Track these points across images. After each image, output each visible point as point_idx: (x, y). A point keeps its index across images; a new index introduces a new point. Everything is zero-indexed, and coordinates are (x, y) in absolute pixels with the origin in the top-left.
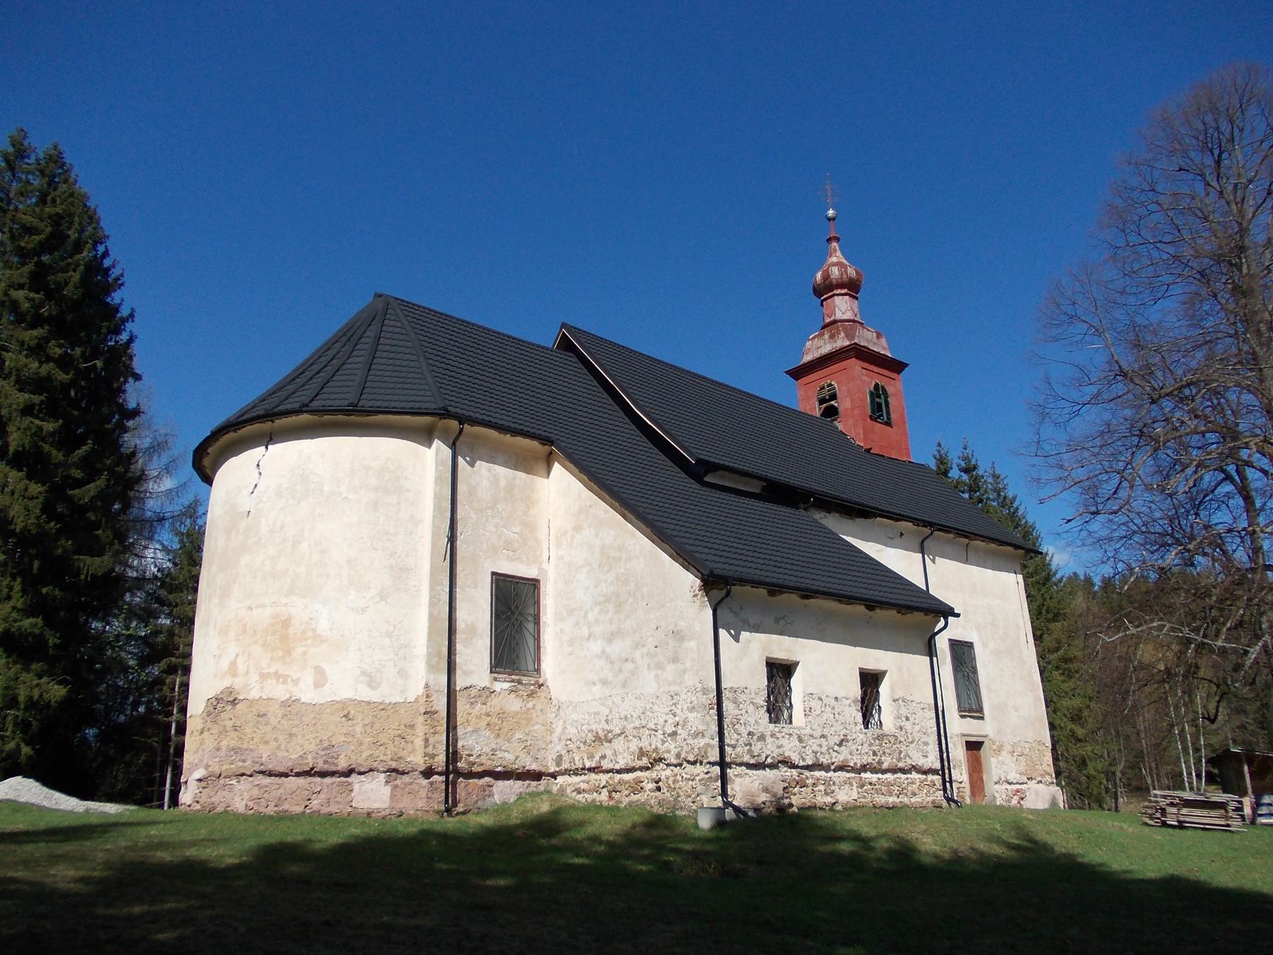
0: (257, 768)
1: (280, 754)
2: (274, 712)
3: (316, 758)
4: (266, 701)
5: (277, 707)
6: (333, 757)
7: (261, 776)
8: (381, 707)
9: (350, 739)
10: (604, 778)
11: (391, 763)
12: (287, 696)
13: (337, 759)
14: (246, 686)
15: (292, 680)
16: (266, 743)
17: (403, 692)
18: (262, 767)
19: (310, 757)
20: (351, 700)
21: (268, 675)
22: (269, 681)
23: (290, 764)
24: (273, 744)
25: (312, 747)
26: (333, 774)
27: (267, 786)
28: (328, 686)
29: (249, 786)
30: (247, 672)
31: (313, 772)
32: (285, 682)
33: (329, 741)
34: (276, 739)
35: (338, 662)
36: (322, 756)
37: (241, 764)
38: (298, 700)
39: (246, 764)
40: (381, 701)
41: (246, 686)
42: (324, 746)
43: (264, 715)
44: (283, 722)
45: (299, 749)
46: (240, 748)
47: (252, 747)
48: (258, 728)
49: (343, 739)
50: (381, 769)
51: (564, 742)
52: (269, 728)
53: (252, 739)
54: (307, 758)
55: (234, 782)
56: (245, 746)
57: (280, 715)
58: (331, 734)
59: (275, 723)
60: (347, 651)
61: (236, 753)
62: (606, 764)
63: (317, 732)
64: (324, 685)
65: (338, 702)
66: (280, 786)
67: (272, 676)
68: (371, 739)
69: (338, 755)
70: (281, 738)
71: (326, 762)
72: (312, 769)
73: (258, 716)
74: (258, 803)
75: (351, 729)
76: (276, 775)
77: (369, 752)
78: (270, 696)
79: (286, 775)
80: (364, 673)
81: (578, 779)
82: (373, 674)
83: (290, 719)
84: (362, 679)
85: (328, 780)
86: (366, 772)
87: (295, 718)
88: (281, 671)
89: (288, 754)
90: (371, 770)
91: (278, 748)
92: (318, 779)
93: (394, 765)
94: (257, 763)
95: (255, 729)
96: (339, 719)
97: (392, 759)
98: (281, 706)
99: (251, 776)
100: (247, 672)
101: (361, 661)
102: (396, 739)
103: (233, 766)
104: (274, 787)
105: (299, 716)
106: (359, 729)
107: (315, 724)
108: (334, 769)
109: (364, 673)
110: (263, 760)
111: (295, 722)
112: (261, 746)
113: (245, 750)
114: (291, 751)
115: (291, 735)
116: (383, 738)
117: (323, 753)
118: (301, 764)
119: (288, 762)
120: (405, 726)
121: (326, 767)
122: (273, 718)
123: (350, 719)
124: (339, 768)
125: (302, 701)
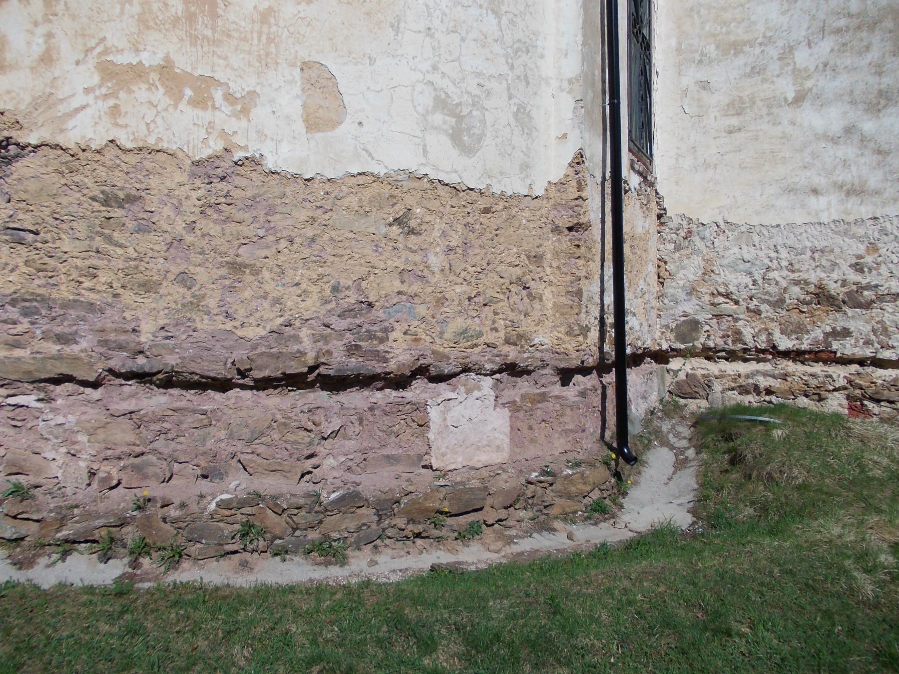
0: (119, 361)
1: (204, 324)
2: (170, 193)
3: (325, 338)
4: (132, 159)
5: (184, 178)
6: (371, 336)
7: (132, 387)
8: (482, 203)
9: (415, 288)
10: (840, 373)
11: (506, 349)
12: (216, 146)
13: (382, 341)
14: (45, 101)
15: (229, 98)
16: (148, 287)
17: (525, 167)
18: (141, 360)
19: (304, 333)
20: (412, 176)
21: (138, 72)
22: (141, 92)
23: (240, 354)
24: (177, 293)
25: (311, 306)
26: (365, 381)
27: (162, 419)
28: (347, 127)
29: (94, 414)
30: (47, 59)
31: (311, 377)
32: (201, 101)
33: (359, 289)
34: (185, 279)
35: (372, 61)
36: (340, 334)
37: (54, 348)
38: (254, 162)
39: (74, 349)
40: (482, 187)
41: (45, 101)
42: (344, 304)
43: (131, 199)
44: (206, 225)
45: (267, 311)
46: (43, 299)
47: (92, 297)
48: (109, 239)
49: (397, 285)
50: (488, 366)
51: (707, 298)
52: (153, 243)
53: (92, 273)
54: (297, 339)
55: (30, 400)
56: (65, 292)
57: (191, 206)
58: (365, 270)
59: (179, 227)
60: (397, 31)
61: (26, 313)
62: (845, 347)
63: (322, 262)
64: (334, 124)
65: (377, 178)
66: (208, 419)
67: (154, 76)
68: (465, 288)
69: (386, 330)
70: (202, 275)
71: (352, 349)
72: (312, 369)
73: (106, 203)
74: (136, 468)
75: (417, 258)
76: (188, 385)
77: (459, 323)
78: (151, 141)
79: (223, 385)
80: (442, 103)
81: (753, 366)
82: (465, 112)
83: (228, 219)
84: (438, 118)
85: (355, 398)
86: (455, 375)
87: (247, 216)
88: (182, 63)
89: (229, 326)
90: (466, 370)
91: (196, 304)
92: (320, 397)
93: (512, 354)
94: (121, 348)
95: (99, 242)
96: (384, 230)
97: (508, 342)
98: (193, 175)
99: (95, 385)
100: (47, 59)
101: (435, 68)
102: (514, 288)
103: (18, 353)
104: (189, 420)
105: (261, 213)
106: (436, 260)
107: (313, 240)
108: (378, 368)
109: (442, 103)
110: (143, 339)
111: (246, 230)
112: (128, 297)
113: (66, 305)
114: (241, 313)
115: (236, 267)
116: (490, 285)
117: (343, 324)
118: (278, 356)
119: (231, 349)
120: (528, 257)
121: (354, 364)
122: (167, 211)
123: (412, 232)
124: (392, 366)
125: (270, 163)
